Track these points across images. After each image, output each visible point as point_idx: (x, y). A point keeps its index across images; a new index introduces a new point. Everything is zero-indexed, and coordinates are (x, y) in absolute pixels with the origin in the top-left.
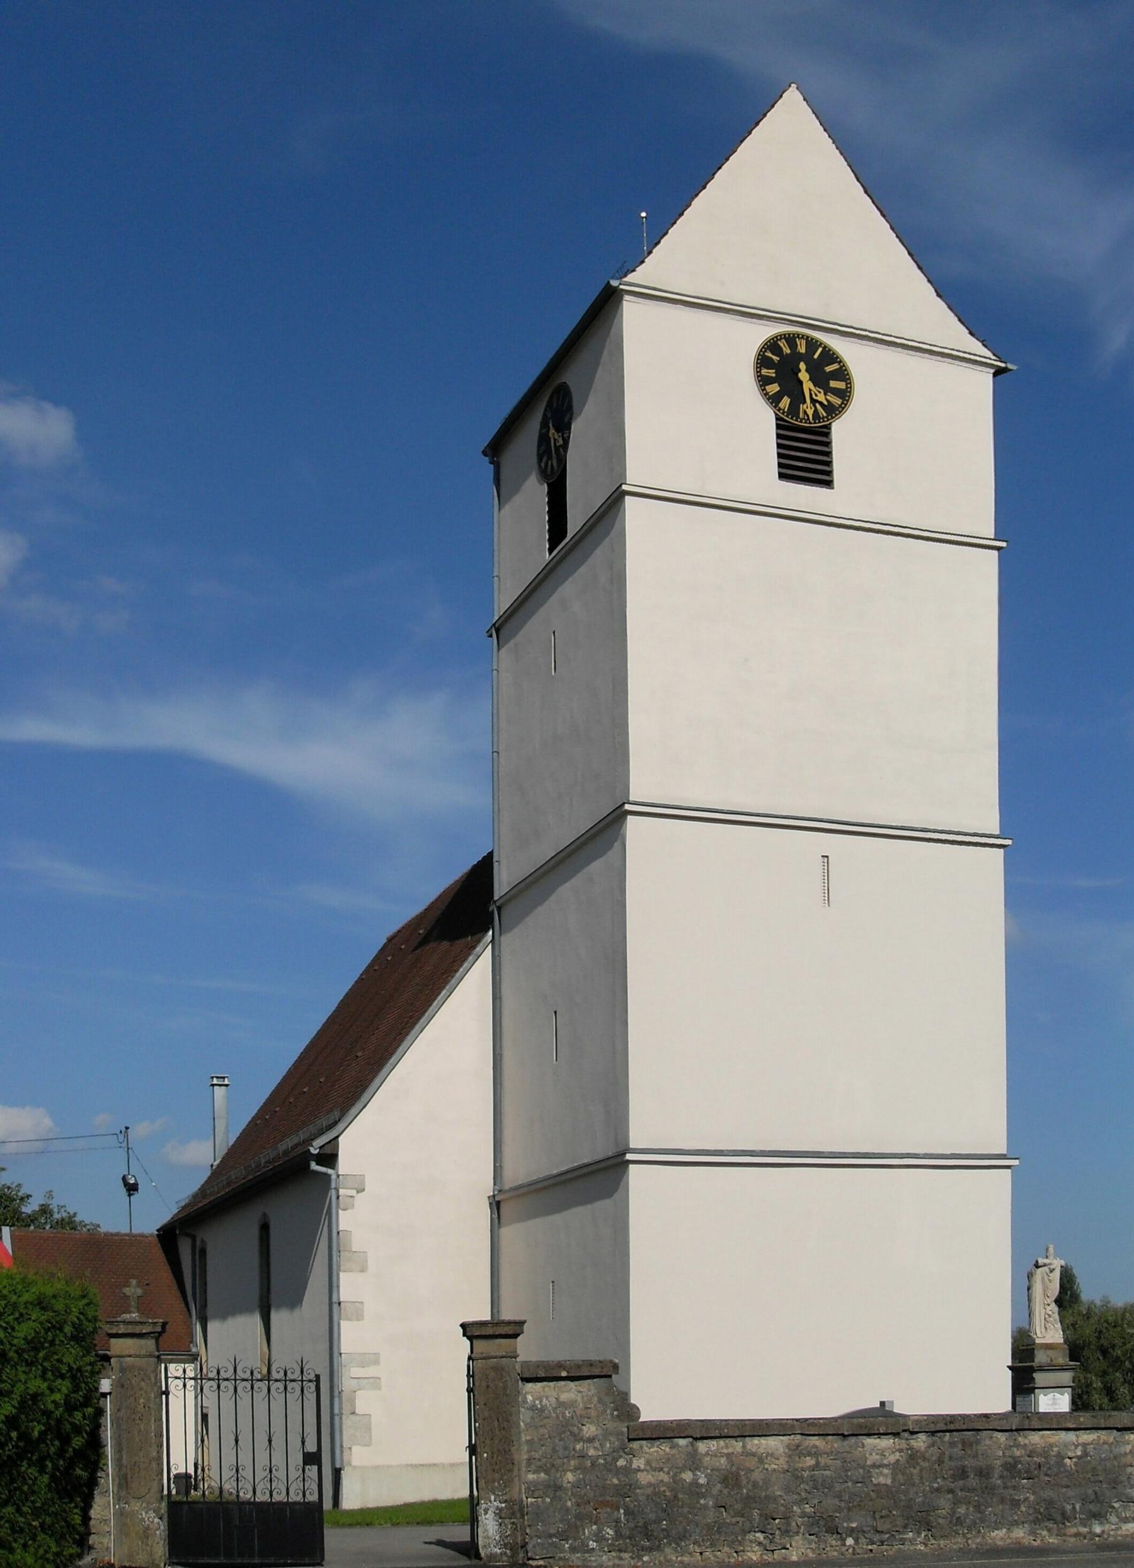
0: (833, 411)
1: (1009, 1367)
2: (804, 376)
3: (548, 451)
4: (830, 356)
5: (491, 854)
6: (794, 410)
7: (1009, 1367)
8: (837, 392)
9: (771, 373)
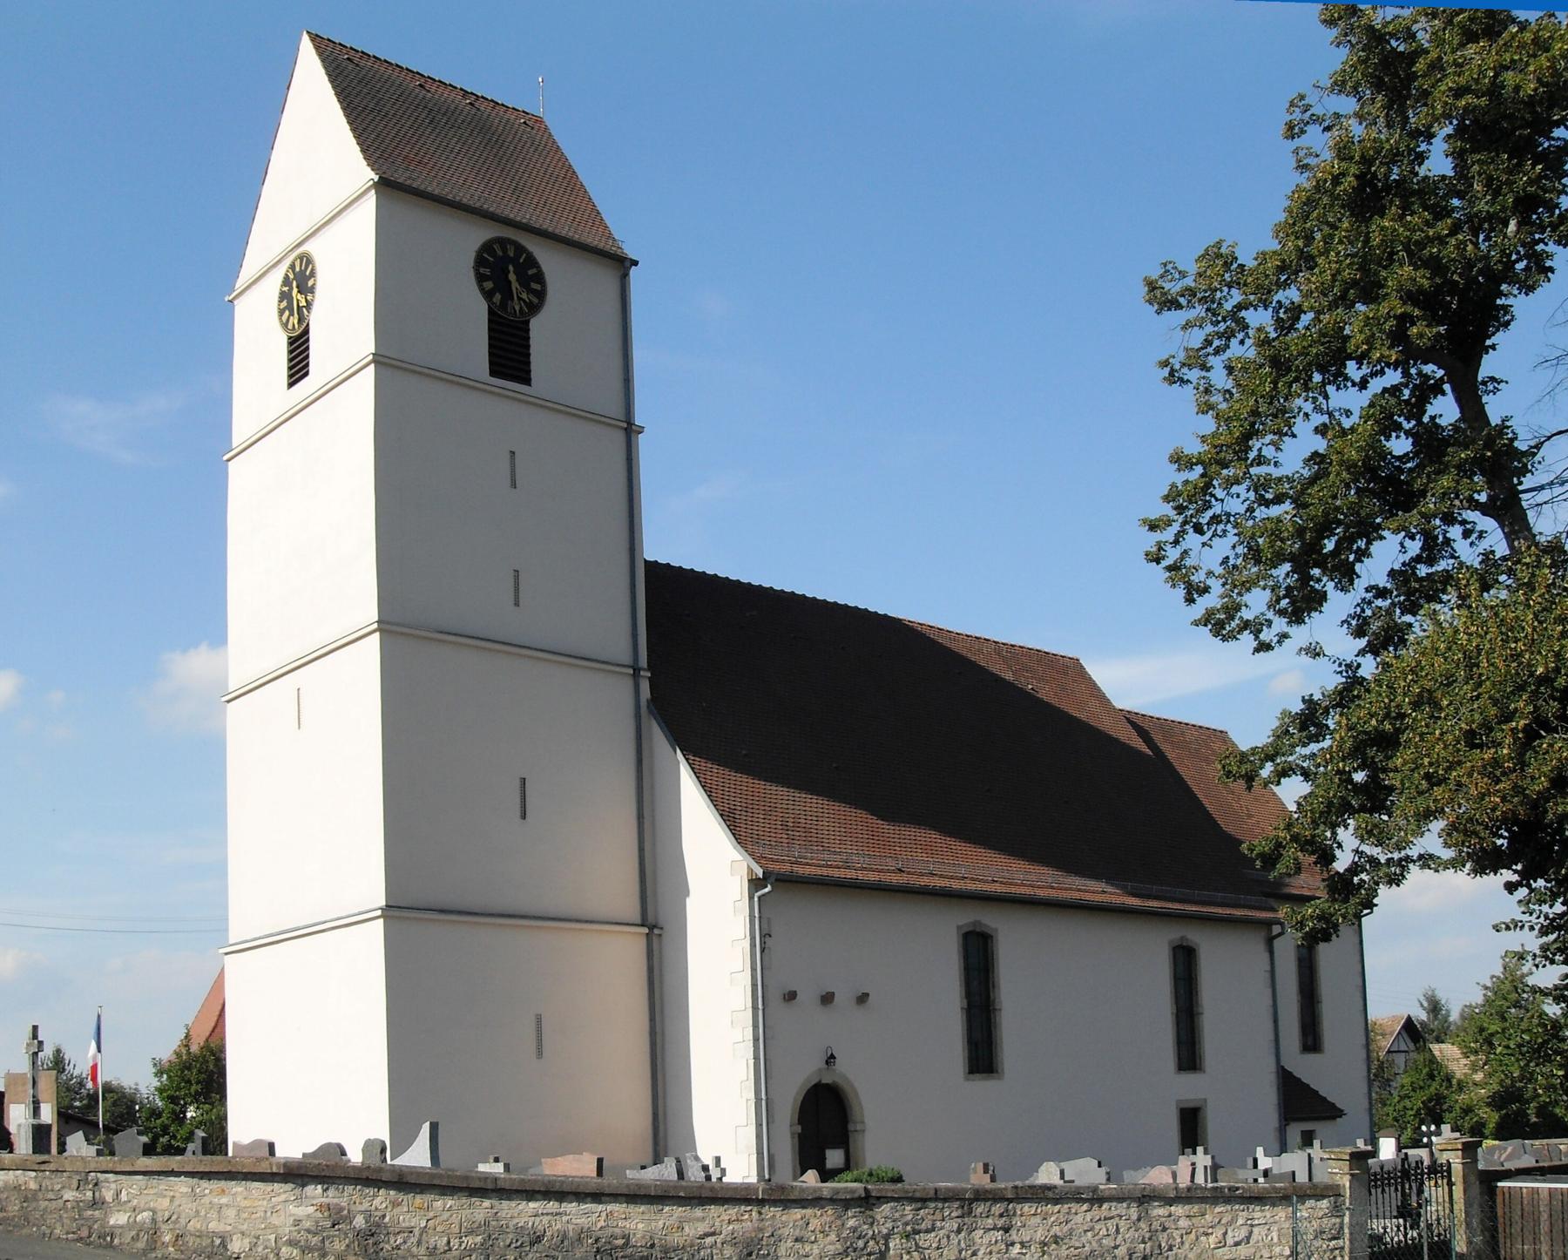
0: (534, 308)
1: (1158, 312)
2: (512, 277)
3: (290, 307)
4: (532, 262)
5: (291, 385)
6: (503, 305)
7: (1158, 312)
8: (534, 292)
9: (487, 271)
